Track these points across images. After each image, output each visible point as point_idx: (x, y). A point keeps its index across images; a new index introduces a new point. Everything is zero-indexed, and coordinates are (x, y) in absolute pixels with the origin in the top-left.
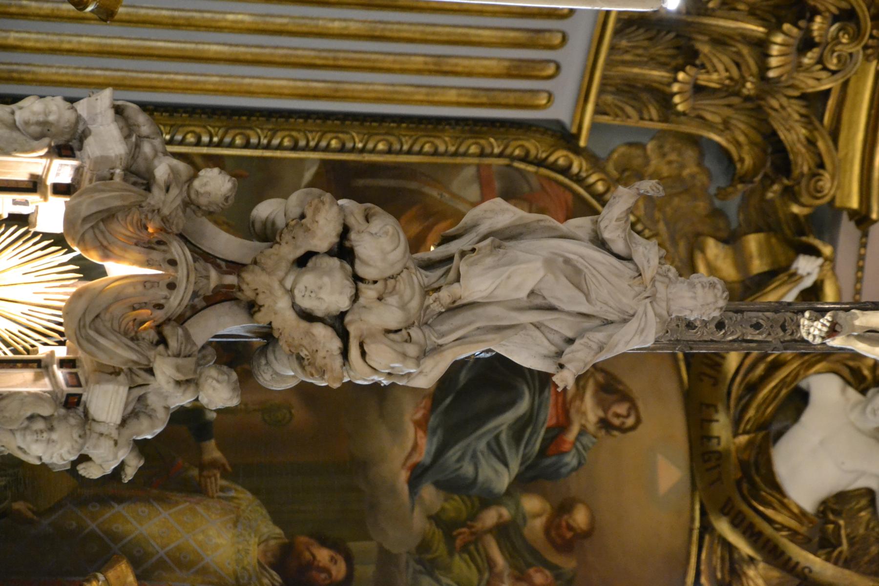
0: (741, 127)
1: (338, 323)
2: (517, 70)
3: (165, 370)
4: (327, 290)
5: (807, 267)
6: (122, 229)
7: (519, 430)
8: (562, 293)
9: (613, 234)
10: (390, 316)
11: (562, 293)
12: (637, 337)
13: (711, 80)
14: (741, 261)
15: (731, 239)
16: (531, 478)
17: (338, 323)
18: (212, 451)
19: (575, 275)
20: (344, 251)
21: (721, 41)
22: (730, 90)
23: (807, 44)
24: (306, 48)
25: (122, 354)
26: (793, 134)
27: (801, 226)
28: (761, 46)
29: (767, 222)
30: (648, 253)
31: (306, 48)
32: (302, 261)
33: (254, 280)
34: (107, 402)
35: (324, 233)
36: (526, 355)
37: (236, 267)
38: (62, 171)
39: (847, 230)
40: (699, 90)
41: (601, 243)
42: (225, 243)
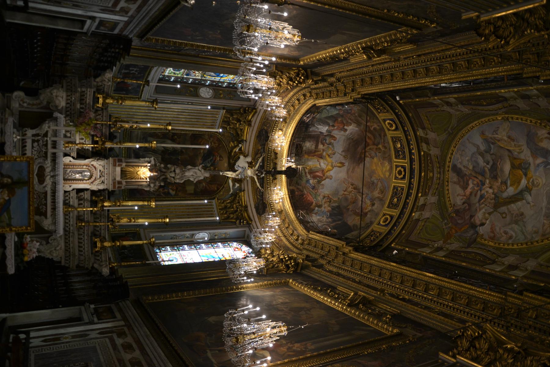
0: (234, 132)
1: (174, 177)
2: (212, 125)
3: (157, 183)
4: (173, 175)
5: (240, 145)
6: (154, 170)
7: (211, 161)
8: (194, 175)
9: (200, 169)
10: (178, 177)
11: (194, 175)
12: (202, 178)
13: (231, 127)
14: (234, 144)
15: (233, 142)
16: (212, 165)
17: (174, 177)
18: (180, 162)
19: (196, 173)
20: (174, 171)
21: (232, 123)
22: (233, 128)
23: (241, 124)
24: (190, 123)
25: (153, 181)
26: (239, 133)
27: (240, 141)
28: (236, 124)
29: (237, 141)
30: (203, 171)
31: (190, 123)
32: (171, 172)
33: (166, 174)
34: (152, 185)
35: (173, 169)
36: (192, 179)
37: (165, 172)
38: (149, 165)
39: (245, 142)
40: (230, 128)
41: (199, 169)
42: (164, 170)
